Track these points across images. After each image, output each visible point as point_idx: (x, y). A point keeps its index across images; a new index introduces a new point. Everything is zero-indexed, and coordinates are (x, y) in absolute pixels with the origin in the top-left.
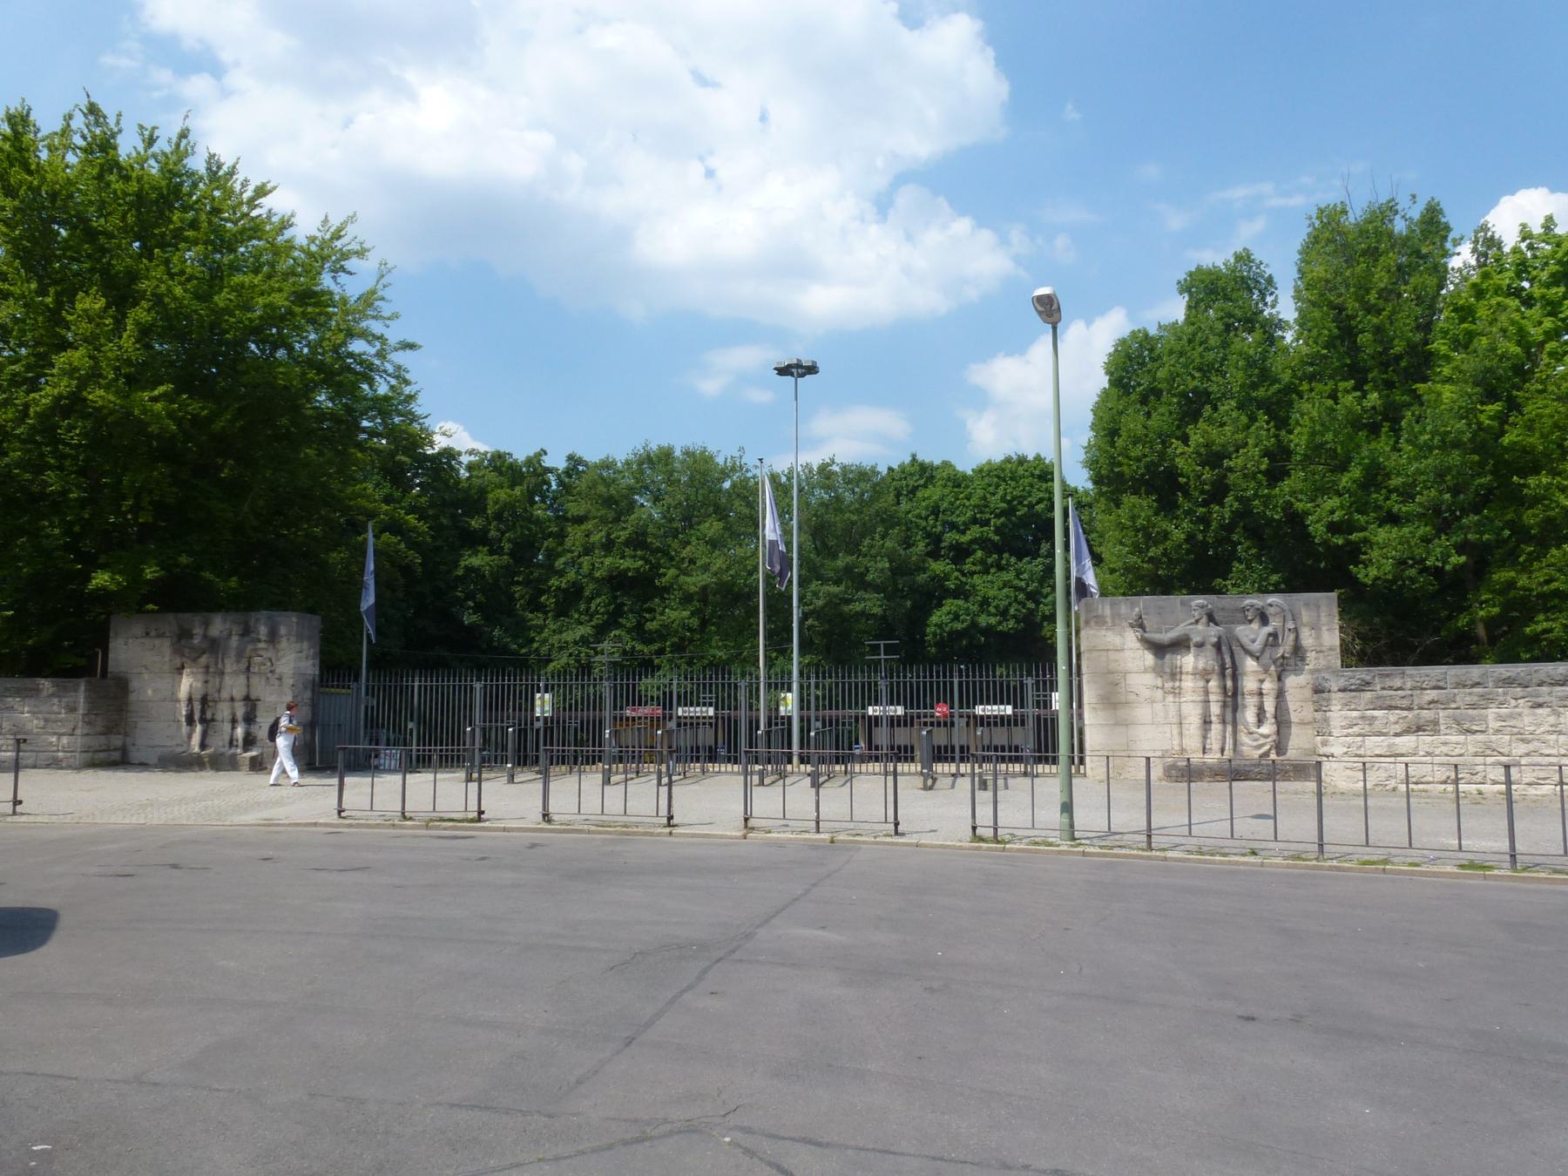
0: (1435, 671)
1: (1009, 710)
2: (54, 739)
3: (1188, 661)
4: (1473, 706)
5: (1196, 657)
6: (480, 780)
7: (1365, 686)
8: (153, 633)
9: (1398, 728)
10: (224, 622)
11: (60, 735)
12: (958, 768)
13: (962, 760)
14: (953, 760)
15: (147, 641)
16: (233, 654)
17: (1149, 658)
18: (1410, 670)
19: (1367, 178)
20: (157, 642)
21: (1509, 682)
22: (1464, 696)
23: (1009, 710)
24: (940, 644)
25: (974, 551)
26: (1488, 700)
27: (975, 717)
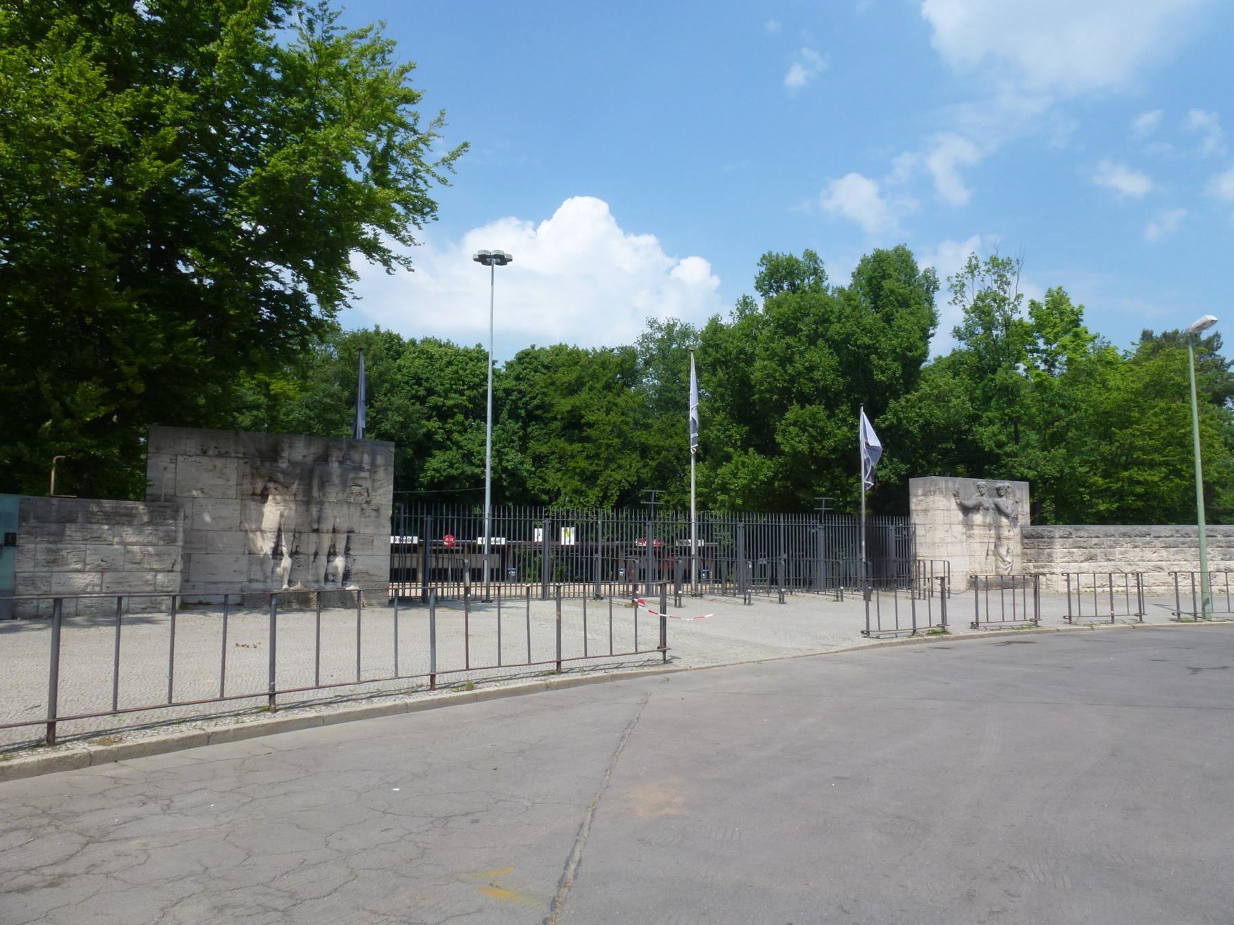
0: (1111, 528)
1: (416, 540)
2: (149, 576)
3: (978, 518)
4: (1111, 547)
5: (984, 516)
6: (499, 608)
7: (1069, 536)
8: (210, 452)
9: (1082, 558)
10: (309, 445)
11: (157, 571)
12: (598, 589)
13: (605, 578)
14: (581, 580)
15: (205, 460)
16: (336, 480)
17: (960, 516)
18: (1086, 527)
19: (861, 257)
20: (219, 462)
21: (1124, 535)
22: (1108, 541)
23: (416, 540)
24: (432, 485)
25: (455, 414)
26: (1116, 543)
27: (475, 545)
